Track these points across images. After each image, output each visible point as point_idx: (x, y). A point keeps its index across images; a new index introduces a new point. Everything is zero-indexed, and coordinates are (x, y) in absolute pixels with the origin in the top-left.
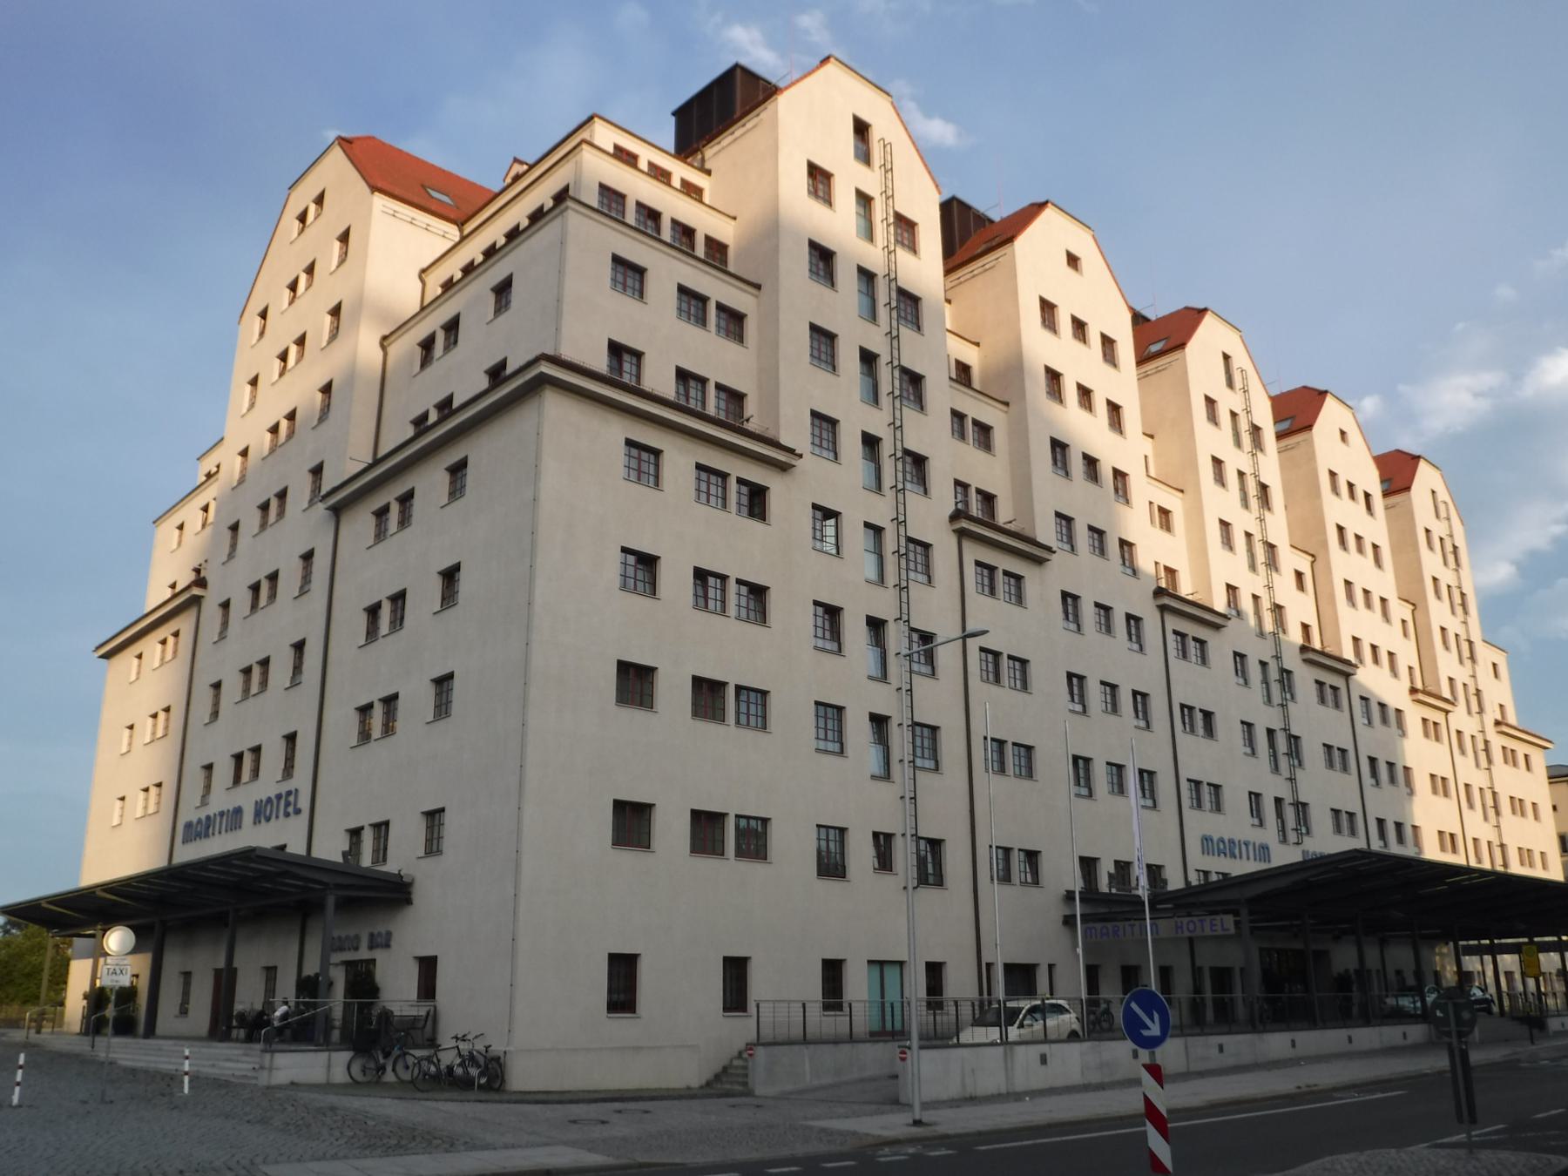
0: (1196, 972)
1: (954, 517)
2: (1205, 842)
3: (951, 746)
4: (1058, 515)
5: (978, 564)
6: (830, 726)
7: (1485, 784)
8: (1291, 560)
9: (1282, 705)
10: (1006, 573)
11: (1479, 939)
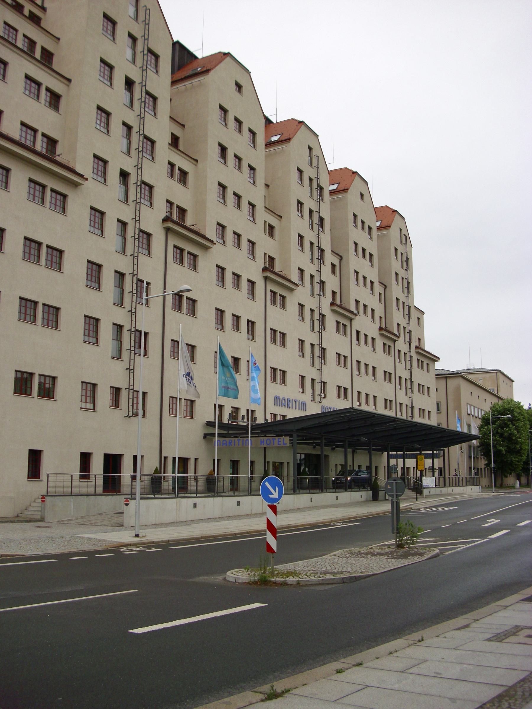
0: (266, 463)
1: (165, 220)
2: (276, 399)
3: (154, 343)
4: (218, 224)
5: (175, 246)
6: (91, 329)
7: (408, 377)
8: (329, 258)
9: (319, 332)
10: (189, 253)
11: (397, 452)
